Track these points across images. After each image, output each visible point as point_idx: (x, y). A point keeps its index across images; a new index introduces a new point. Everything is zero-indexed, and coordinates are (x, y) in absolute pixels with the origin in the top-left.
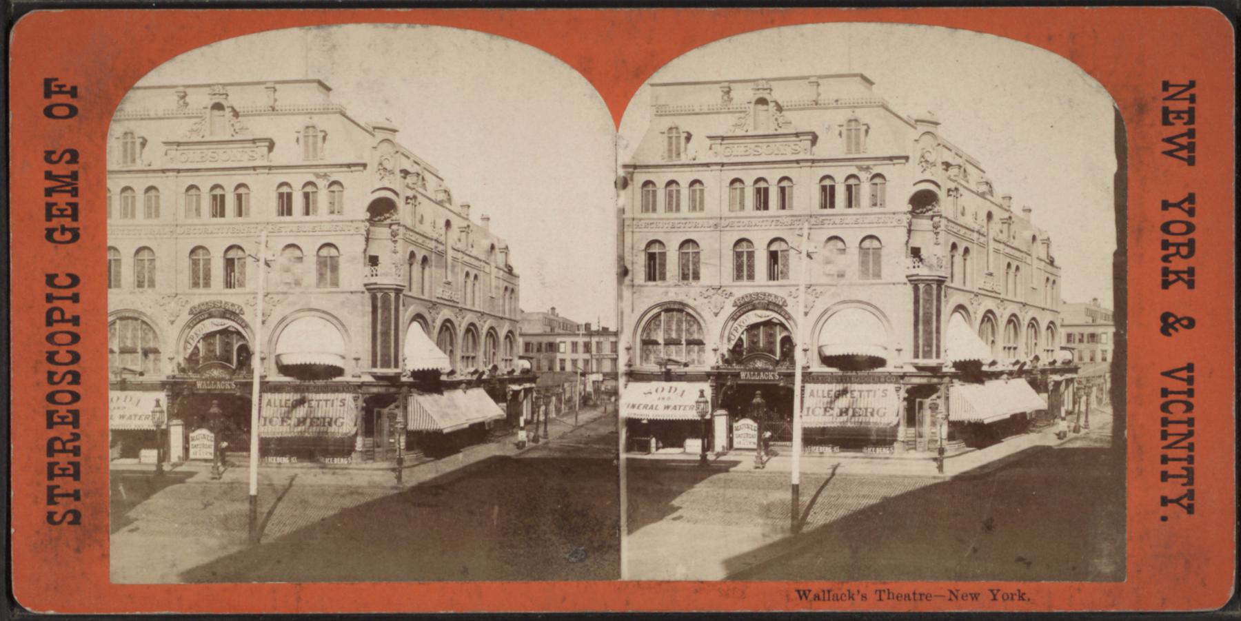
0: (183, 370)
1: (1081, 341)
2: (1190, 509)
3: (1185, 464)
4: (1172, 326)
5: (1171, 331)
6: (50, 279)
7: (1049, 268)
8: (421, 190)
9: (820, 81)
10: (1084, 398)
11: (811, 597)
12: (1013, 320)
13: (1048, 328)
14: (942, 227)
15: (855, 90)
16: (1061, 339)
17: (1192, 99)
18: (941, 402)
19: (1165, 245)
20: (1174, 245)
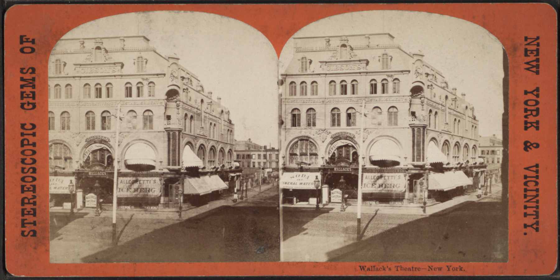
0: (83, 167)
1: (488, 154)
2: (537, 230)
3: (535, 209)
4: (529, 147)
5: (528, 149)
6: (23, 126)
7: (473, 121)
8: (190, 86)
9: (370, 37)
10: (489, 180)
11: (366, 269)
12: (457, 144)
13: (473, 148)
14: (425, 102)
15: (386, 41)
16: (479, 153)
17: (538, 45)
18: (425, 181)
19: (526, 110)
20: (529, 110)
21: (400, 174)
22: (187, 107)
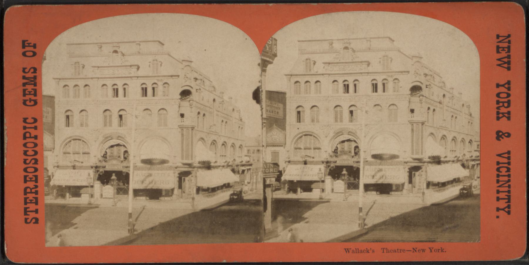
2: (509, 213)
3: (507, 194)
4: (501, 136)
5: (500, 138)
6: (25, 120)
7: (240, 122)
9: (141, 43)
11: (351, 251)
14: (424, 100)
15: (154, 48)
16: (245, 151)
17: (509, 42)
18: (424, 173)
19: (498, 102)
21: (168, 172)
22: (199, 106)
